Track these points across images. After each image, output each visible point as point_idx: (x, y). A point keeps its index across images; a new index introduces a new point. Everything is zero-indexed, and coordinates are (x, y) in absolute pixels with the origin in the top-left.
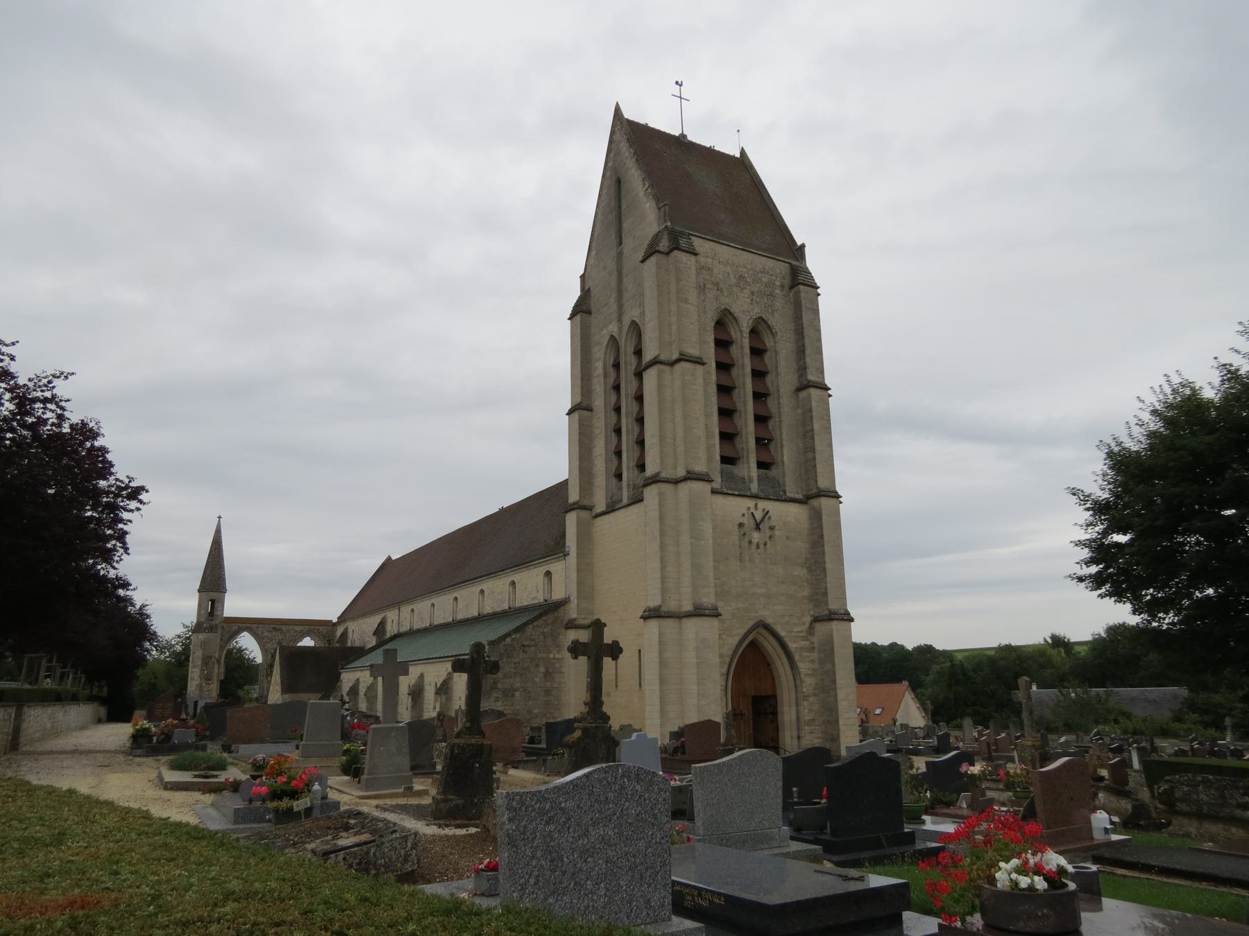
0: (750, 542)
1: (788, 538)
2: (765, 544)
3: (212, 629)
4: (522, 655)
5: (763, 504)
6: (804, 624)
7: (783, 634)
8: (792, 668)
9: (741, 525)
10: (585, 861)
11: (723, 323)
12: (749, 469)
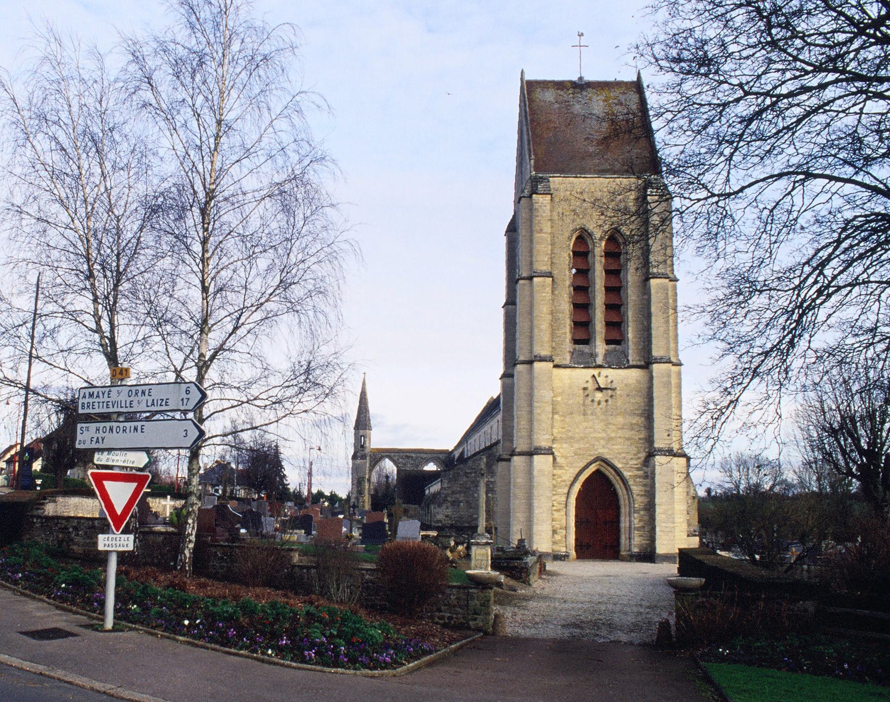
0: (593, 401)
1: (628, 395)
2: (607, 401)
3: (363, 457)
4: (465, 479)
5: (604, 372)
6: (639, 458)
7: (619, 466)
8: (627, 489)
9: (585, 389)
10: (483, 621)
11: (583, 238)
12: (601, 347)
